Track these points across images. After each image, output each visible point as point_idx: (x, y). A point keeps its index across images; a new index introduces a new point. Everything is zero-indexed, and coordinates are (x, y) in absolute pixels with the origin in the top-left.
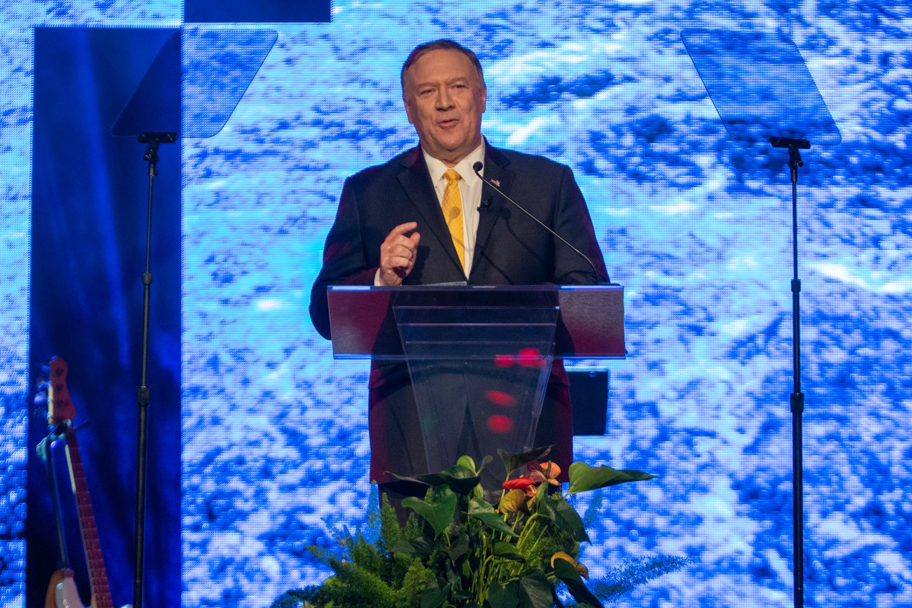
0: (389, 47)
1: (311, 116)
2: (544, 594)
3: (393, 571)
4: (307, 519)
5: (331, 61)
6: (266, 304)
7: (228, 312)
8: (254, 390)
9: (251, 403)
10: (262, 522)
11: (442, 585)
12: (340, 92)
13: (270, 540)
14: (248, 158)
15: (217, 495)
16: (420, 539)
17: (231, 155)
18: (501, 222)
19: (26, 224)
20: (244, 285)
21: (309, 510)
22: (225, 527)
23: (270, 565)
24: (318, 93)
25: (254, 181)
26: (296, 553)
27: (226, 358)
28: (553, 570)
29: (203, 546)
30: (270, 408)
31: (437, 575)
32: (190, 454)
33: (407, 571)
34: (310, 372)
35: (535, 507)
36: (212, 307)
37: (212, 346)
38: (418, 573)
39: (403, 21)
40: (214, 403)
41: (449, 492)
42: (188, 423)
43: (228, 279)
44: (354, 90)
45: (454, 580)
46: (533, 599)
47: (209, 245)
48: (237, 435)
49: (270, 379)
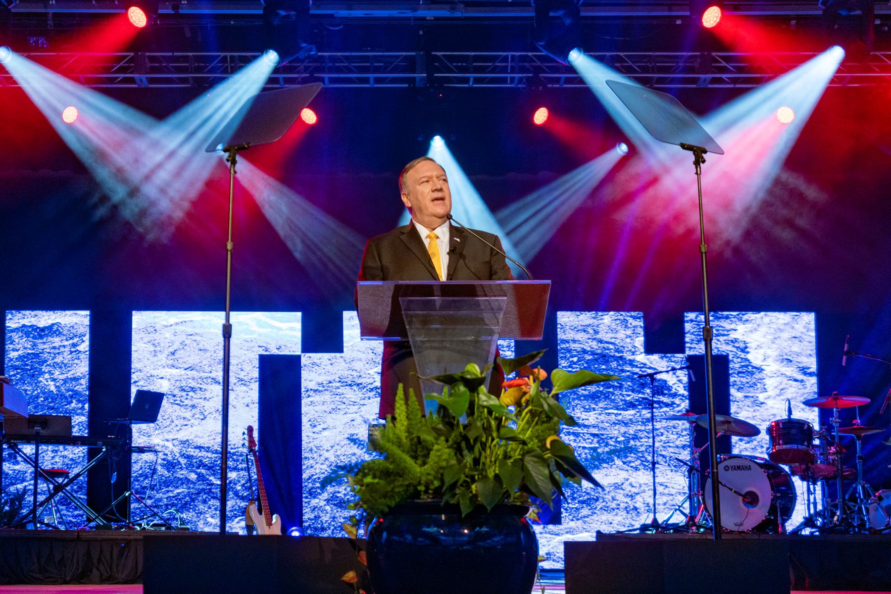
0: (360, 360)
1: (338, 380)
2: (541, 468)
3: (419, 450)
4: (338, 495)
5: (343, 363)
6: (325, 433)
7: (315, 436)
8: (323, 458)
9: (321, 462)
10: (325, 496)
11: (460, 462)
12: (346, 373)
13: (328, 501)
14: (320, 391)
15: (312, 488)
16: (440, 426)
17: (315, 391)
18: (461, 261)
19: (257, 410)
20: (319, 428)
21: (339, 492)
22: (315, 498)
23: (328, 508)
24: (340, 373)
25: (322, 399)
26: (334, 505)
27: (314, 449)
28: (548, 450)
29: (309, 503)
30: (327, 462)
31: (456, 454)
32: (305, 476)
33: (432, 450)
34: (339, 453)
35: (527, 403)
36: (311, 434)
37: (311, 445)
38: (441, 452)
39: (364, 353)
40: (311, 461)
41: (462, 388)
42: (304, 467)
43: (315, 426)
44: (350, 372)
45: (469, 459)
46: (534, 474)
47: (310, 416)
48: (318, 471)
49: (327, 455)
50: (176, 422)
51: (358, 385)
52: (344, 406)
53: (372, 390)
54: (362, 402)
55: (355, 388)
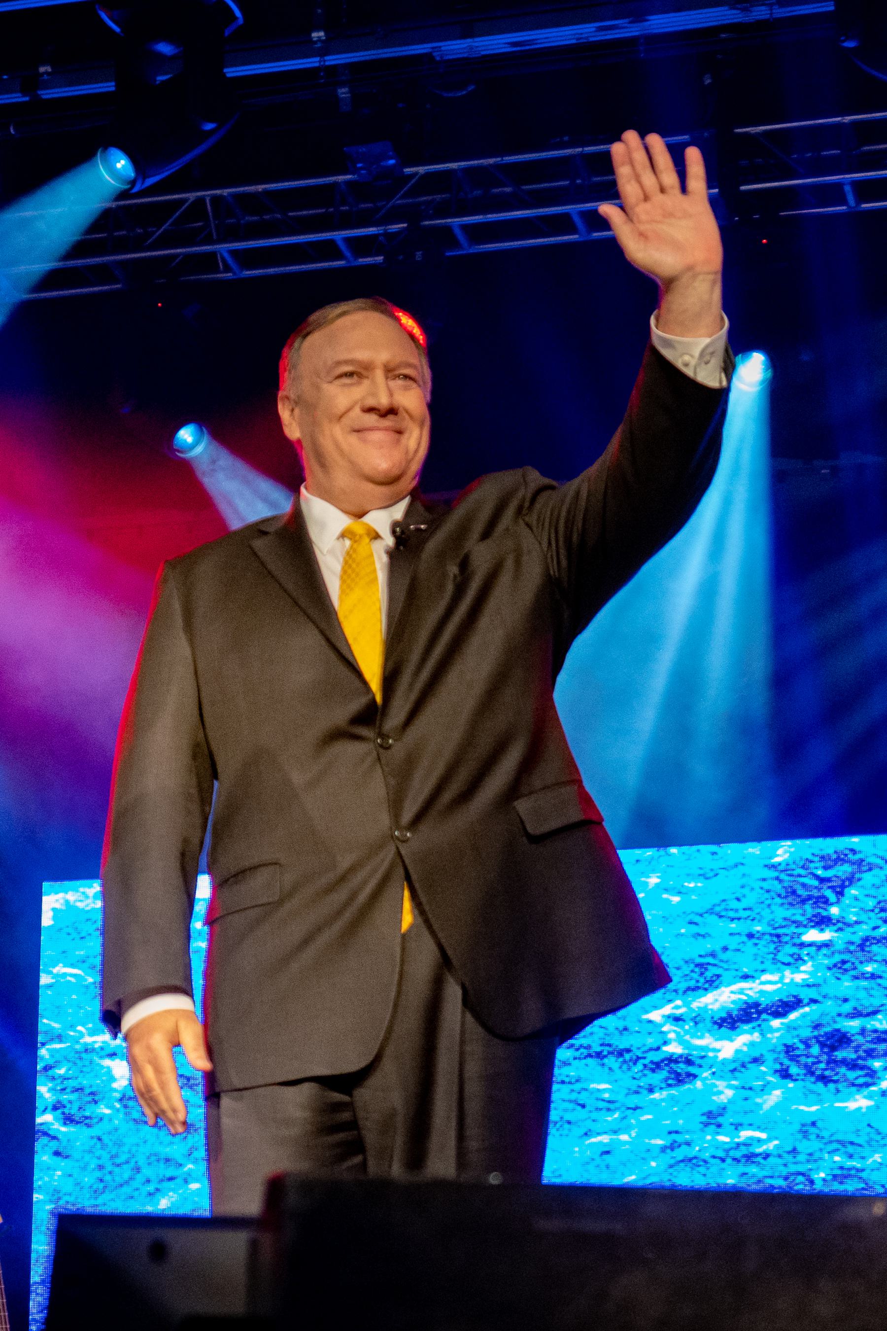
50: (147, 1172)
51: (621, 1053)
52: (581, 1113)
53: (656, 1066)
54: (633, 1100)
55: (611, 1061)
